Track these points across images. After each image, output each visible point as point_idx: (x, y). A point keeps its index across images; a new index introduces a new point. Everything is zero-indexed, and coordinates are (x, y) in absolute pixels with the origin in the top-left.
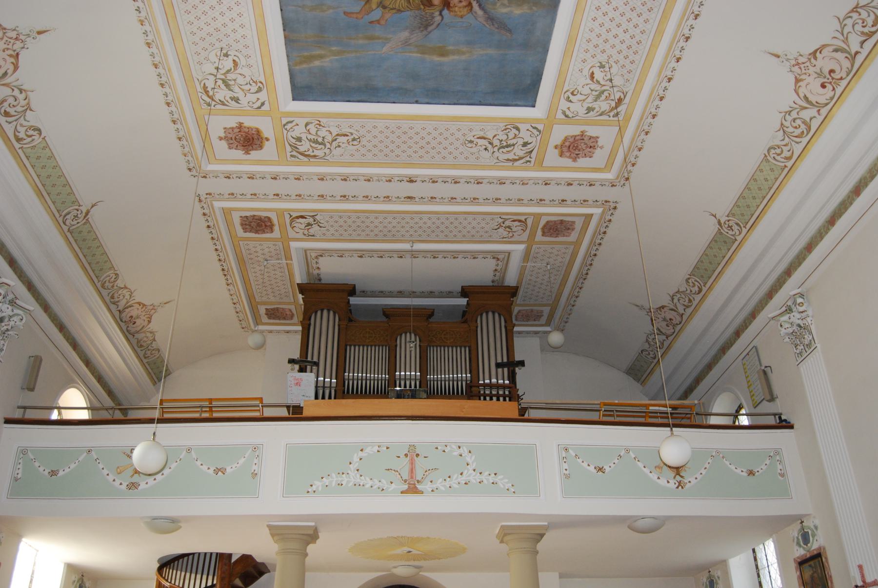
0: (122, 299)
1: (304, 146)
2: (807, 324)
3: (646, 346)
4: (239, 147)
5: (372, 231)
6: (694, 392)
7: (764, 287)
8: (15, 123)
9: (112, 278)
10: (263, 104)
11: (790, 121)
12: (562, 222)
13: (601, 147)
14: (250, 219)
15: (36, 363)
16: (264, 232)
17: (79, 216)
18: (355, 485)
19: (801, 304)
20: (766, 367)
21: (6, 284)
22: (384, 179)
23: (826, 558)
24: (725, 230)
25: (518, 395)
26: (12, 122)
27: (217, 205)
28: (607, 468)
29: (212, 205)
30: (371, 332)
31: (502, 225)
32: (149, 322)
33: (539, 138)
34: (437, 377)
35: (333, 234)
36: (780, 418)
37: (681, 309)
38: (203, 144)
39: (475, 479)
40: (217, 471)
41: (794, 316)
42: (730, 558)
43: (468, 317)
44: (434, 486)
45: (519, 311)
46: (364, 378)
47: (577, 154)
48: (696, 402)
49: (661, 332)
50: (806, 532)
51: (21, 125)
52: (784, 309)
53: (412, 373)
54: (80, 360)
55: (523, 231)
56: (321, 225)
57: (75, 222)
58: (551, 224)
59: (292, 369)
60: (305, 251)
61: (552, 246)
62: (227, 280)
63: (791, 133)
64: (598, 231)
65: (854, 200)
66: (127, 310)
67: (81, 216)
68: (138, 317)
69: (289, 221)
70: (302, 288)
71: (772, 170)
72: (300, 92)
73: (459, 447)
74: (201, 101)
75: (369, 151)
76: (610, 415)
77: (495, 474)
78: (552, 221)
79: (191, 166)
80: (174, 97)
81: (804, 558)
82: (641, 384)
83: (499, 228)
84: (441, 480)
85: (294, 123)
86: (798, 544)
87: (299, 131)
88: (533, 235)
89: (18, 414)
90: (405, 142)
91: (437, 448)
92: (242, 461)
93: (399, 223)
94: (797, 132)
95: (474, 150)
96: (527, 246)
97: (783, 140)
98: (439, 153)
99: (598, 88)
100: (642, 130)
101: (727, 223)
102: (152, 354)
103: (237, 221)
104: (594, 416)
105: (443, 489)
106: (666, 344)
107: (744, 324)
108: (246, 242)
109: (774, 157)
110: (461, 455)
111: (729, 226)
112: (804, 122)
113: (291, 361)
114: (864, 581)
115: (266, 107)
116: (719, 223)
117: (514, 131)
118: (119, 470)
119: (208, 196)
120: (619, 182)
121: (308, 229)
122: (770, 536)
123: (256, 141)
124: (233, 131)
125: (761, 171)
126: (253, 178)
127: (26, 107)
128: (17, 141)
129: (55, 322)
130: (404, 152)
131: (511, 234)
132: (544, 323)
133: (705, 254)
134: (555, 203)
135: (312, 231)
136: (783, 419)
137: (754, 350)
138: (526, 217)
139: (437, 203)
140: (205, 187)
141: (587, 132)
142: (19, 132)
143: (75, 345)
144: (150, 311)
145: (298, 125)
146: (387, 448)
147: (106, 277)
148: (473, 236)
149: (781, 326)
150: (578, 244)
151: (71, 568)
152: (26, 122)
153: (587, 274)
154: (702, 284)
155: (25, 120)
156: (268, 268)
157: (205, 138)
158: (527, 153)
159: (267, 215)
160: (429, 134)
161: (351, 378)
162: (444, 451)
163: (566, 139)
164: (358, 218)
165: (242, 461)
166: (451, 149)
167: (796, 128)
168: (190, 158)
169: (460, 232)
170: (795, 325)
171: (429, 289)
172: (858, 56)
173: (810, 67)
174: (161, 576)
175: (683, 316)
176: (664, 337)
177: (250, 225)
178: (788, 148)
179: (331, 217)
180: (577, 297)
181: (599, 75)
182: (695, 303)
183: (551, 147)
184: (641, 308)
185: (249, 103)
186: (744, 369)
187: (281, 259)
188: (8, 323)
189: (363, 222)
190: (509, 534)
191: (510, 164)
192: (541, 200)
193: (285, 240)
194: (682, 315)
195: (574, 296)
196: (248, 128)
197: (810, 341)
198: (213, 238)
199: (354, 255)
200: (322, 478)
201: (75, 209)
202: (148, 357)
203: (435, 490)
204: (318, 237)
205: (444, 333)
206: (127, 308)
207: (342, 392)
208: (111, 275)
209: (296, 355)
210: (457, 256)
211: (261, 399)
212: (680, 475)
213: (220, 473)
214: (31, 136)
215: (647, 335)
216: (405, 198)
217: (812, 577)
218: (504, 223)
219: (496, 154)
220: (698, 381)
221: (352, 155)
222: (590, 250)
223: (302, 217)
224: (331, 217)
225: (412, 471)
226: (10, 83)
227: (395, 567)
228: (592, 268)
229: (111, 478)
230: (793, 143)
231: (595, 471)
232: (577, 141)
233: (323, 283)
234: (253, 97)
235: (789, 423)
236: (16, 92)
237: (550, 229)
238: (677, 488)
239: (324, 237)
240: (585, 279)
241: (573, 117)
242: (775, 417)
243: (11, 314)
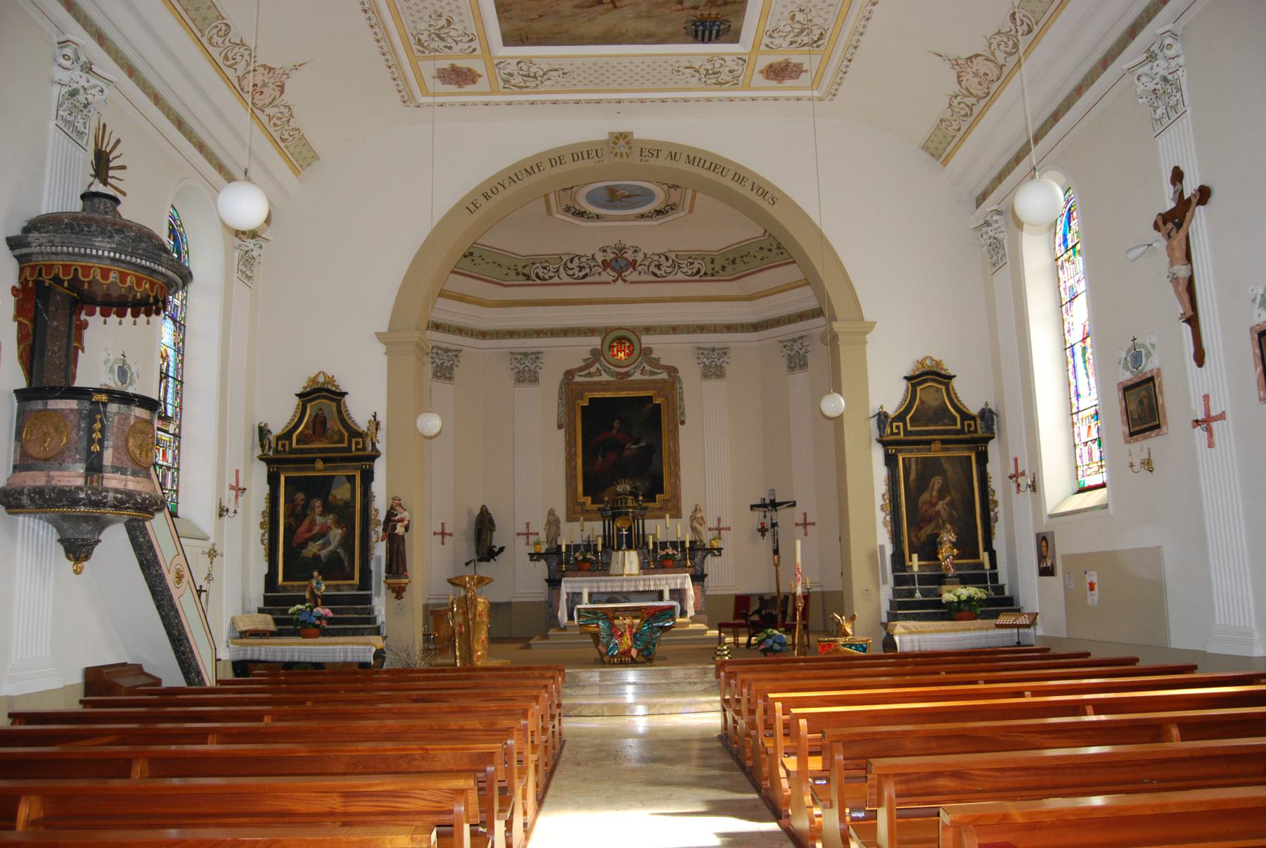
9: (220, 30)
10: (474, 50)
49: (971, 93)
72: (508, 40)
82: (942, 163)
99: (800, 26)
115: (478, 52)
154: (1034, 22)
175: (1004, 68)
181: (799, 17)
208: (220, 26)
215: (949, 98)
234: (465, 46)
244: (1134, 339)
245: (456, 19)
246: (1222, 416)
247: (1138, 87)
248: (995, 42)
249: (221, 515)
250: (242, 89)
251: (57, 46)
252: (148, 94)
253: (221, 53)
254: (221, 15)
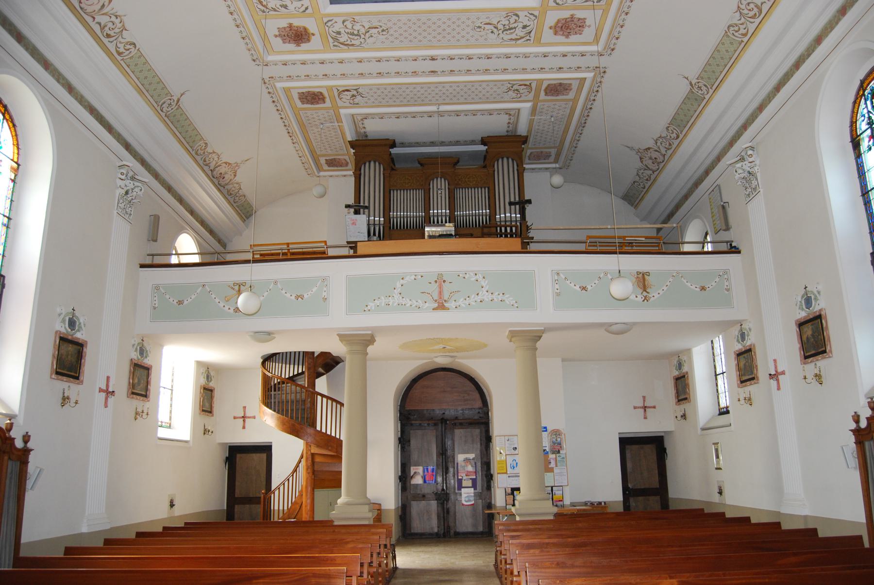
0: (212, 161)
1: (344, 38)
2: (754, 172)
3: (637, 178)
4: (291, 41)
5: (405, 98)
6: (675, 216)
7: (727, 137)
8: (115, 42)
10: (307, 8)
11: (745, 4)
12: (561, 84)
13: (589, 26)
14: (306, 94)
15: (155, 220)
16: (318, 103)
18: (399, 305)
19: (751, 156)
20: (724, 203)
21: (127, 166)
22: (411, 59)
23: (755, 353)
24: (695, 90)
25: (528, 225)
26: (113, 41)
27: (279, 85)
28: (589, 288)
29: (275, 86)
30: (410, 178)
31: (511, 88)
32: (235, 176)
33: (536, 21)
34: (463, 214)
35: (373, 102)
36: (731, 245)
37: (663, 151)
38: (263, 44)
39: (488, 298)
40: (297, 297)
41: (745, 165)
42: (694, 347)
43: (487, 161)
44: (458, 304)
45: (531, 153)
46: (405, 216)
47: (569, 33)
48: (675, 225)
49: (648, 168)
50: (808, 297)
51: (120, 43)
52: (739, 158)
53: (443, 211)
54: (186, 211)
55: (528, 93)
56: (363, 95)
57: (170, 109)
58: (552, 86)
59: (349, 213)
60: (353, 115)
61: (555, 103)
62: (292, 139)
63: (747, 14)
64: (592, 90)
65: (794, 73)
66: (217, 169)
67: (174, 104)
68: (226, 173)
69: (337, 94)
70: (353, 144)
71: (731, 43)
73: (476, 274)
74: (257, 9)
75: (396, 38)
76: (594, 246)
77: (503, 294)
78: (552, 84)
79: (255, 58)
80: (235, 7)
81: (741, 351)
82: (634, 208)
83: (509, 91)
84: (462, 300)
85: (333, 21)
86: (738, 341)
87: (338, 27)
88: (537, 96)
89: (148, 261)
90: (425, 31)
91: (459, 276)
92: (314, 289)
93: (426, 91)
94: (751, 14)
95: (483, 33)
96: (533, 104)
97: (740, 20)
98: (454, 37)
100: (623, 11)
101: (697, 84)
102: (239, 200)
103: (296, 97)
104: (582, 247)
105: (464, 306)
106: (653, 177)
107: (712, 166)
108: (304, 112)
109: (733, 33)
110: (477, 281)
111: (699, 87)
112: (757, 6)
113: (348, 206)
114: (776, 371)
115: (309, 11)
116: (691, 83)
117: (515, 17)
118: (226, 299)
119: (270, 79)
120: (607, 52)
121: (353, 99)
122: (720, 333)
123: (304, 37)
124: (285, 30)
125: (723, 44)
126: (305, 64)
127: (122, 29)
128: (119, 55)
129: (164, 186)
130: (425, 37)
131: (519, 96)
132: (552, 161)
133: (680, 108)
134: (554, 70)
135: (356, 101)
136: (733, 246)
137: (717, 187)
138: (530, 82)
139: (455, 75)
140: (268, 72)
141: (575, 15)
142: (119, 48)
143: (181, 200)
144: (234, 168)
145: (337, 22)
146: (422, 276)
147: (198, 146)
148: (488, 98)
149: (736, 171)
150: (575, 101)
151: (199, 364)
152: (123, 40)
153: (585, 123)
155: (122, 38)
156: (324, 129)
157: (264, 38)
158: (526, 33)
159: (321, 91)
160: (444, 23)
161: (395, 216)
162: (464, 278)
163: (559, 21)
164: (393, 89)
165: (314, 289)
166: (463, 33)
167: (750, 10)
168: (253, 52)
169: (477, 95)
170: (746, 172)
171: (457, 139)
174: (265, 368)
175: (665, 156)
176: (651, 172)
177: (306, 99)
178: (744, 26)
179: (371, 90)
180: (578, 141)
182: (674, 147)
183: (546, 28)
184: (632, 149)
185: (295, 8)
186: (710, 202)
187: (334, 122)
188: (132, 195)
189: (396, 92)
190: (515, 336)
191: (514, 42)
192: (542, 69)
193: (336, 108)
194: (664, 155)
195: (576, 140)
196: (297, 27)
197: (756, 186)
198: (278, 110)
199: (392, 116)
200: (374, 300)
201: (169, 99)
202: (237, 202)
203: (458, 306)
204: (362, 105)
205: (468, 177)
206: (217, 167)
207: (388, 228)
208: (202, 145)
209: (351, 201)
210: (476, 114)
211: (325, 242)
212: (646, 291)
213: (300, 299)
214: (128, 50)
216: (429, 72)
217: (745, 365)
218: (512, 87)
219: (501, 36)
220: (677, 207)
221: (383, 42)
222: (586, 105)
223: (348, 91)
224: (371, 90)
225: (440, 293)
226: (107, 13)
227: (436, 357)
228: (589, 119)
229: (221, 305)
230: (748, 22)
231: (579, 290)
232: (569, 22)
233: (369, 139)
235: (738, 249)
236: (113, 19)
237: (552, 90)
238: (644, 301)
239: (367, 105)
240: (584, 127)
241: (563, 4)
242: (727, 244)
243: (133, 187)
244: (806, 288)
246: (783, 373)
247: (736, 175)
248: (117, 21)
253: (202, 158)
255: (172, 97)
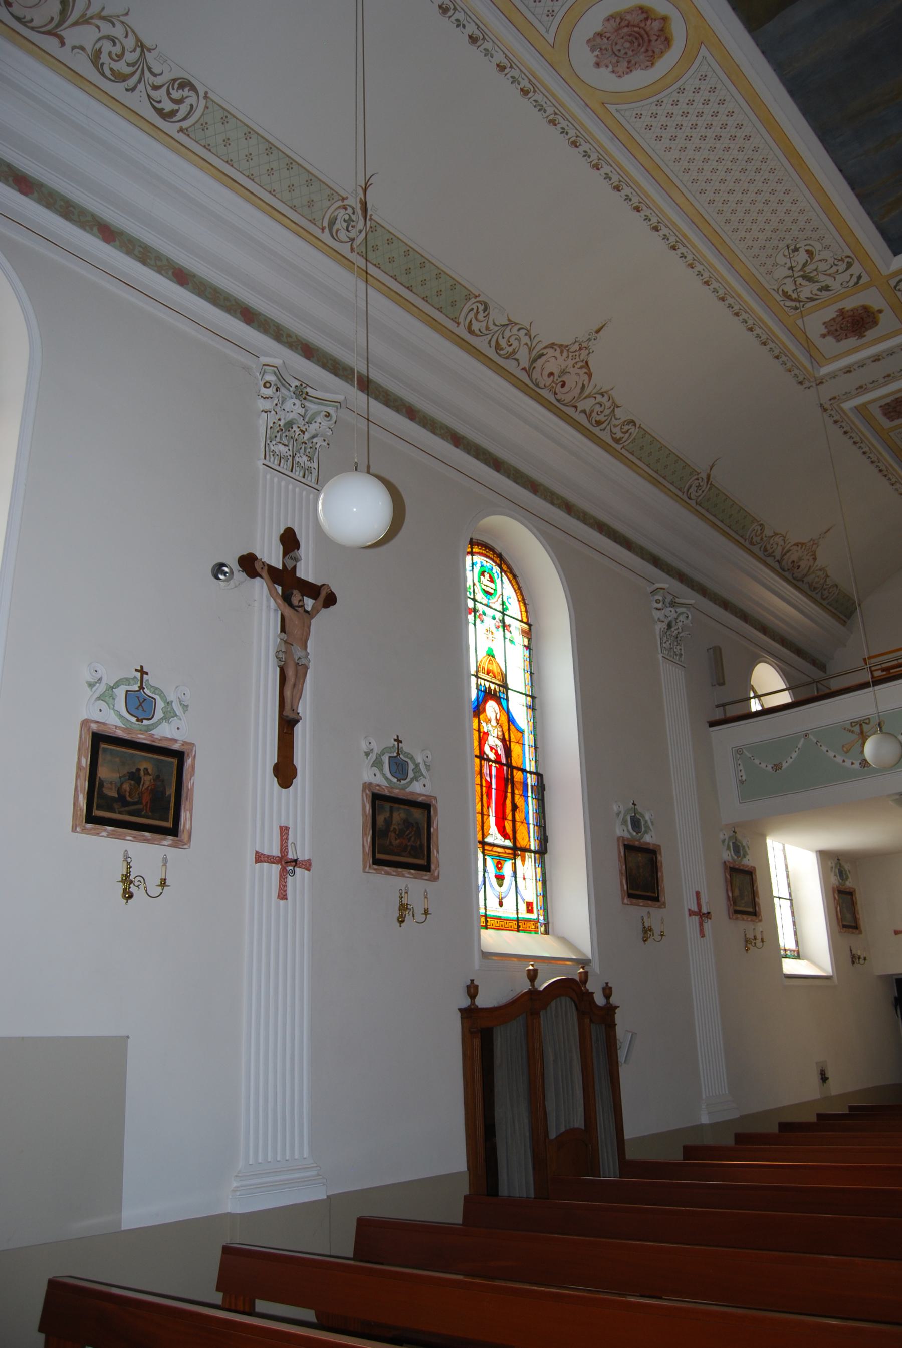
8: (141, 87)
9: (477, 312)
10: (859, 277)
17: (354, 217)
51: (156, 88)
112: (514, 352)
115: (865, 279)
127: (612, 407)
154: (185, 124)
155: (155, 75)
172: (55, 41)
173: (574, 361)
201: (339, 207)
208: (756, 528)
234: (846, 276)
245: (818, 246)
248: (118, 31)
249: (853, 962)
250: (537, 385)
251: (650, 595)
252: (397, 409)
254: (755, 519)
255: (346, 202)
